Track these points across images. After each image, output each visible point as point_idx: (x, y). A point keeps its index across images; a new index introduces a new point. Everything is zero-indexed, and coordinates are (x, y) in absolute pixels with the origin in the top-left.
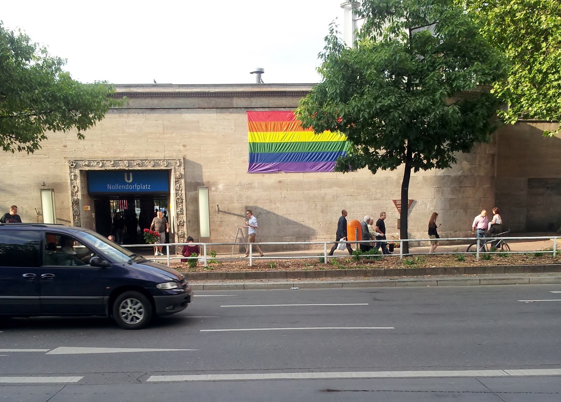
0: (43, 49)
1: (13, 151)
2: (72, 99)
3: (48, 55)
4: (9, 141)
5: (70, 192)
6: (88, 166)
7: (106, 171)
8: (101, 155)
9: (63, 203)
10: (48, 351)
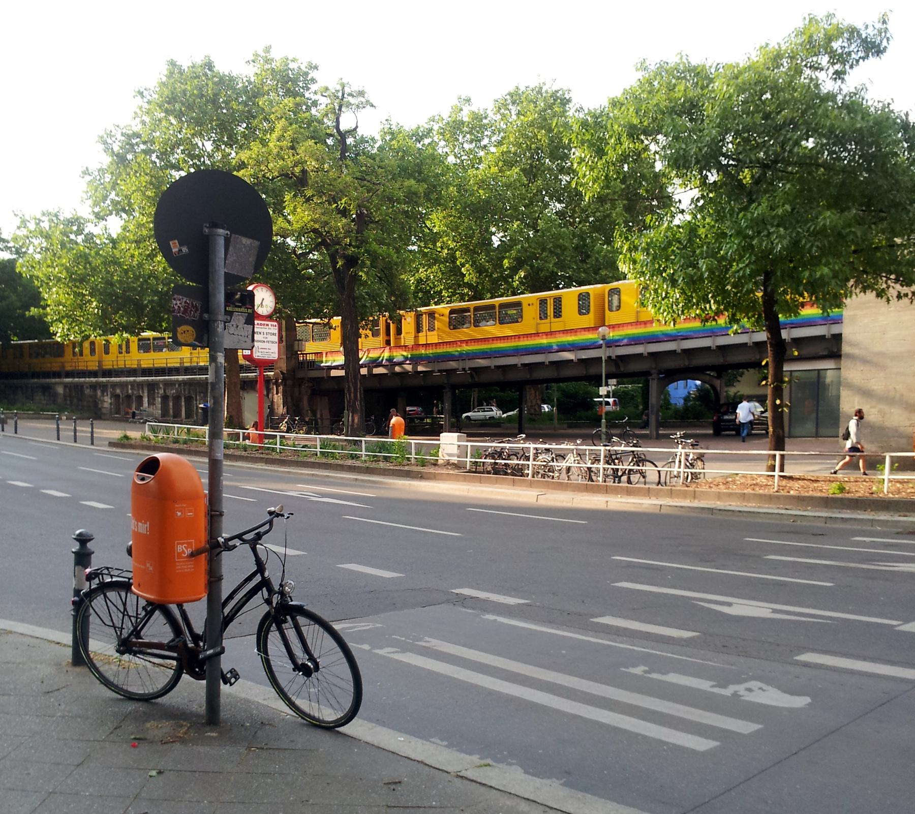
1: (888, 300)
4: (884, 286)
10: (899, 625)
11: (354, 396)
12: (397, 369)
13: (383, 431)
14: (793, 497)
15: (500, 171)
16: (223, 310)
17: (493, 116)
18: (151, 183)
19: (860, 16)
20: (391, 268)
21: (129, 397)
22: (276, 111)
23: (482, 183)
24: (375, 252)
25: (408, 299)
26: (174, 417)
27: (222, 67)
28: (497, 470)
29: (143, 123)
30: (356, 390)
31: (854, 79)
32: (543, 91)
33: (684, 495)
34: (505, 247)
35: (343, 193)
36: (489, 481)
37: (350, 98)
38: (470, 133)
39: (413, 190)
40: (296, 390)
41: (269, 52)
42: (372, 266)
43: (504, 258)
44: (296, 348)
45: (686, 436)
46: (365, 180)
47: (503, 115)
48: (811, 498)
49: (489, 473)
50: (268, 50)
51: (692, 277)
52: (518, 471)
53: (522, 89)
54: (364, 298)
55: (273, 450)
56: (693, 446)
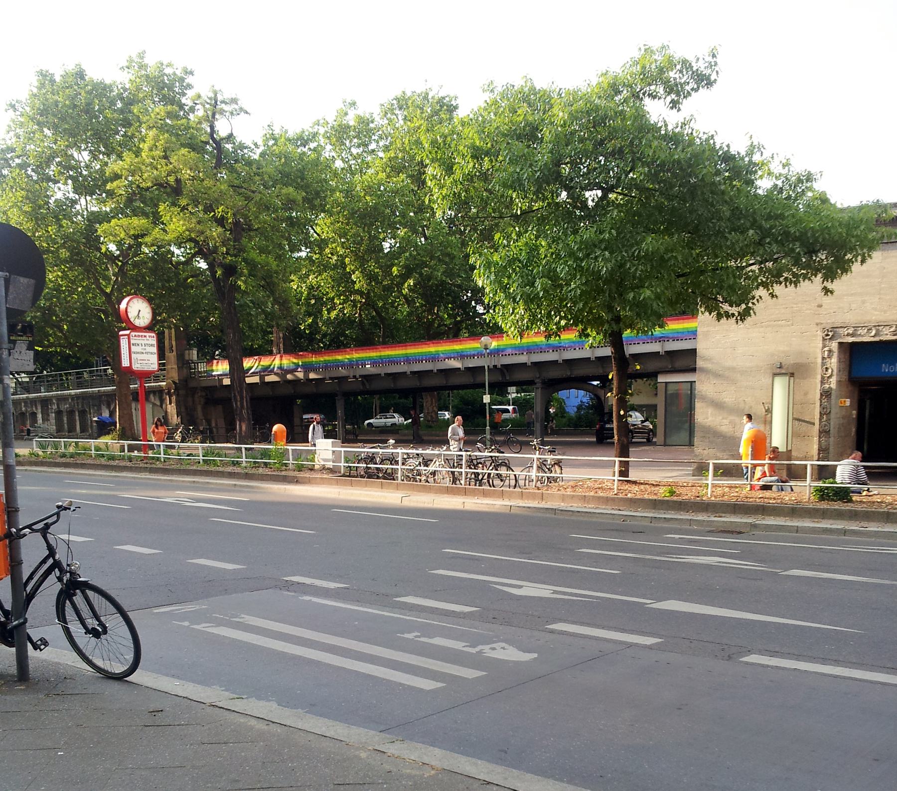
0: (784, 161)
2: (813, 235)
3: (791, 169)
5: (819, 377)
6: (853, 335)
7: (881, 342)
8: (875, 317)
9: (806, 394)
11: (242, 406)
12: (289, 377)
13: (266, 438)
14: (631, 500)
15: (388, 177)
16: (6, 339)
17: (379, 121)
18: (27, 198)
19: (689, 48)
20: (271, 277)
21: (23, 414)
22: (148, 121)
23: (369, 190)
24: (253, 260)
25: (291, 307)
26: (69, 432)
27: (94, 74)
28: (370, 475)
29: (18, 137)
30: (242, 398)
31: (688, 106)
32: (430, 97)
33: (533, 496)
34: (394, 255)
35: (218, 202)
36: (359, 484)
37: (223, 105)
38: (358, 137)
39: (291, 197)
40: (190, 399)
41: (142, 58)
42: (250, 275)
43: (393, 265)
44: (187, 358)
45: (543, 443)
46: (242, 187)
47: (390, 120)
48: (642, 500)
49: (362, 477)
50: (141, 56)
51: (529, 295)
52: (390, 476)
53: (409, 94)
54: (249, 306)
55: (158, 459)
56: (551, 452)
